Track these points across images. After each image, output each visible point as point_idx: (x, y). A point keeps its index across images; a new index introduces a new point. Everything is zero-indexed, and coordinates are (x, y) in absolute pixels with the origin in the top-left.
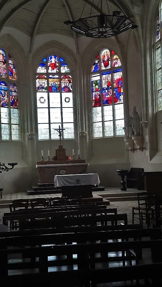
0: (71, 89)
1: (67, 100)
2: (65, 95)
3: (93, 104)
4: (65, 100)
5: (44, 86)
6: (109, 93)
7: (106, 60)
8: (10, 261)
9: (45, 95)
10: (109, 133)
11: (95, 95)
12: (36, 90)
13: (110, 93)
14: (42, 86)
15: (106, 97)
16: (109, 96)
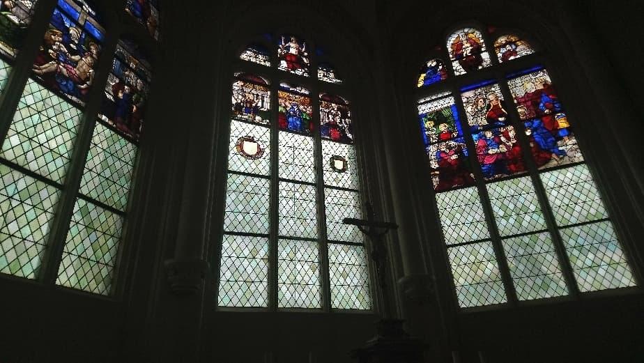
0: (350, 136)
1: (339, 164)
2: (330, 148)
3: (436, 181)
4: (332, 164)
5: (260, 104)
6: (503, 139)
7: (468, 52)
8: (281, 85)
9: (262, 133)
10: (309, 298)
11: (439, 153)
12: (230, 113)
13: (509, 139)
14: (254, 105)
15: (490, 152)
16: (503, 149)
